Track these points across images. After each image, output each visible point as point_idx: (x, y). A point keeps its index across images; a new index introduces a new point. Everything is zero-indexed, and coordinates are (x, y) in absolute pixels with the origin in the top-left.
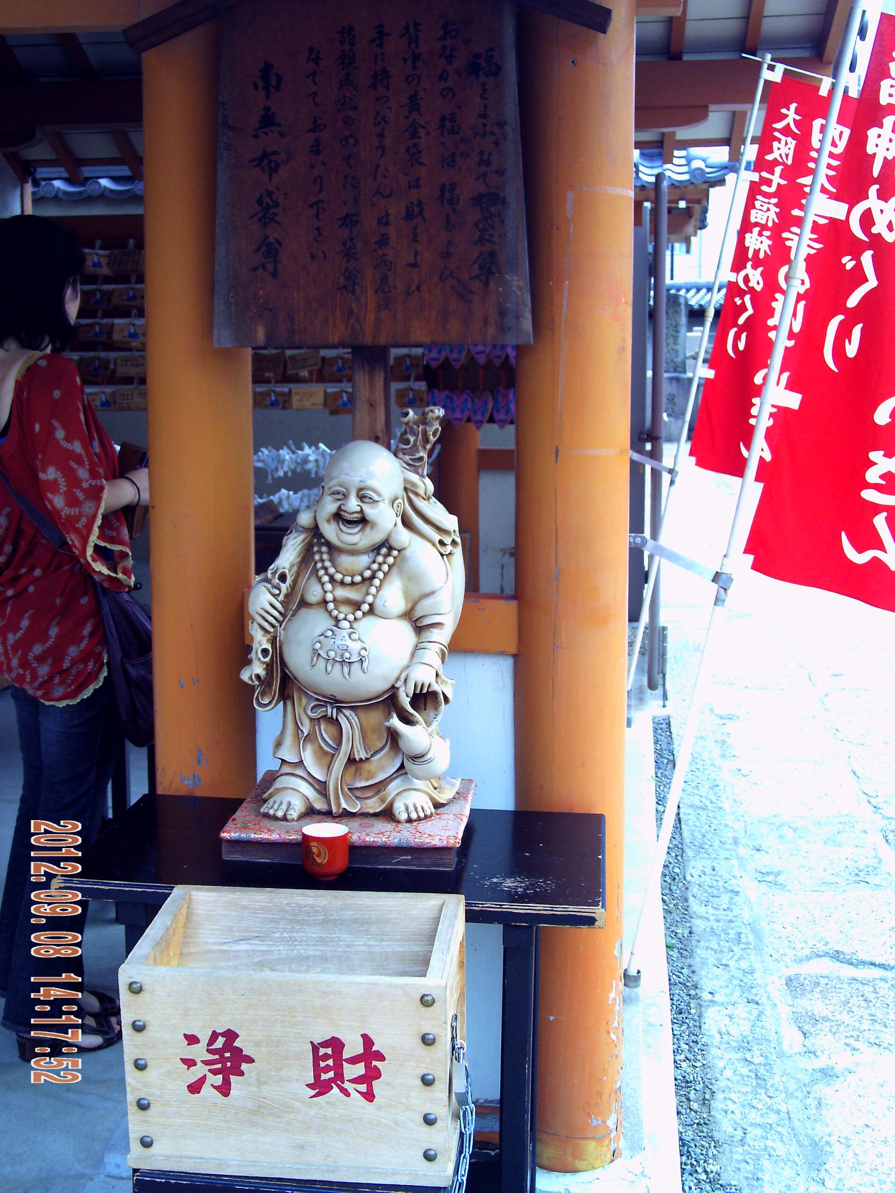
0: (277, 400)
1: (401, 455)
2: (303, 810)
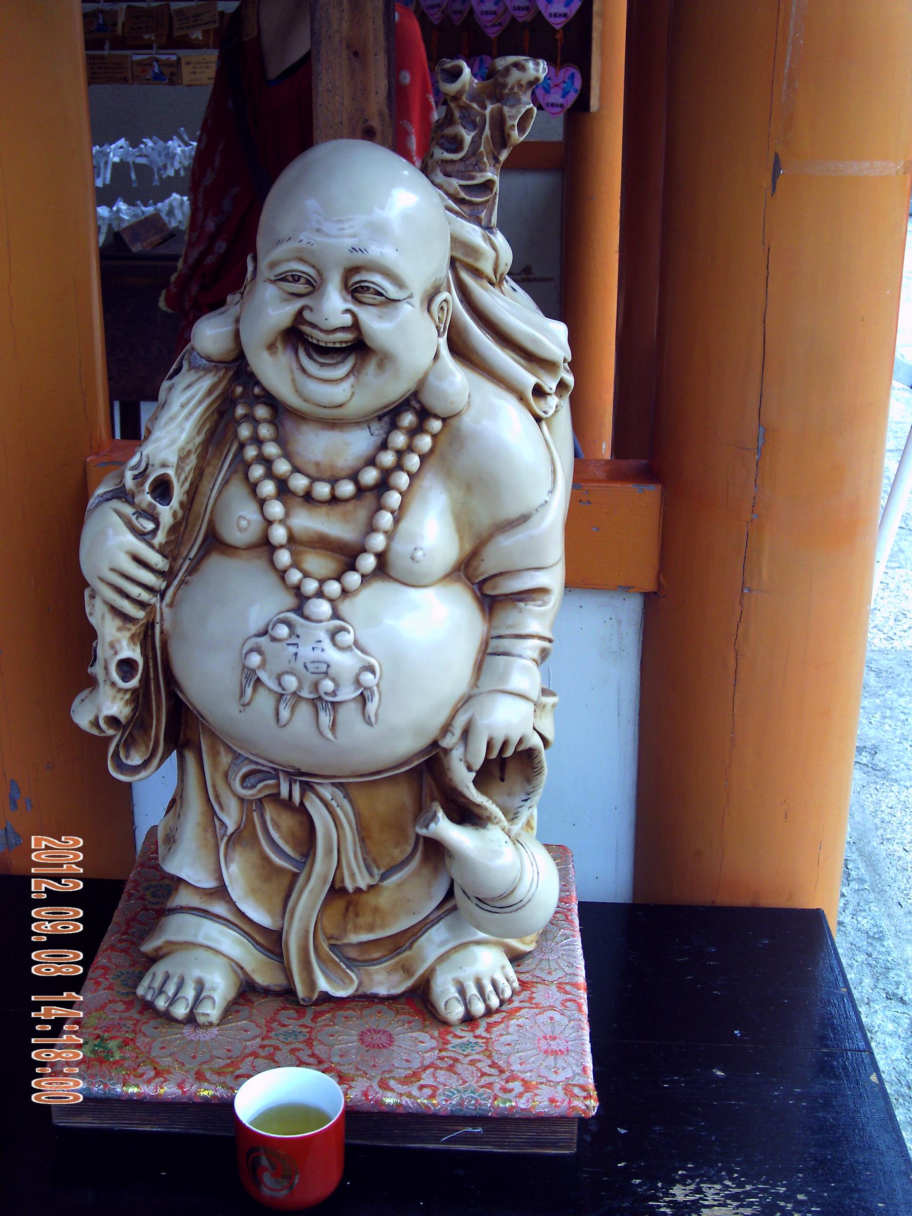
0: (161, 73)
1: (440, 178)
2: (232, 994)
